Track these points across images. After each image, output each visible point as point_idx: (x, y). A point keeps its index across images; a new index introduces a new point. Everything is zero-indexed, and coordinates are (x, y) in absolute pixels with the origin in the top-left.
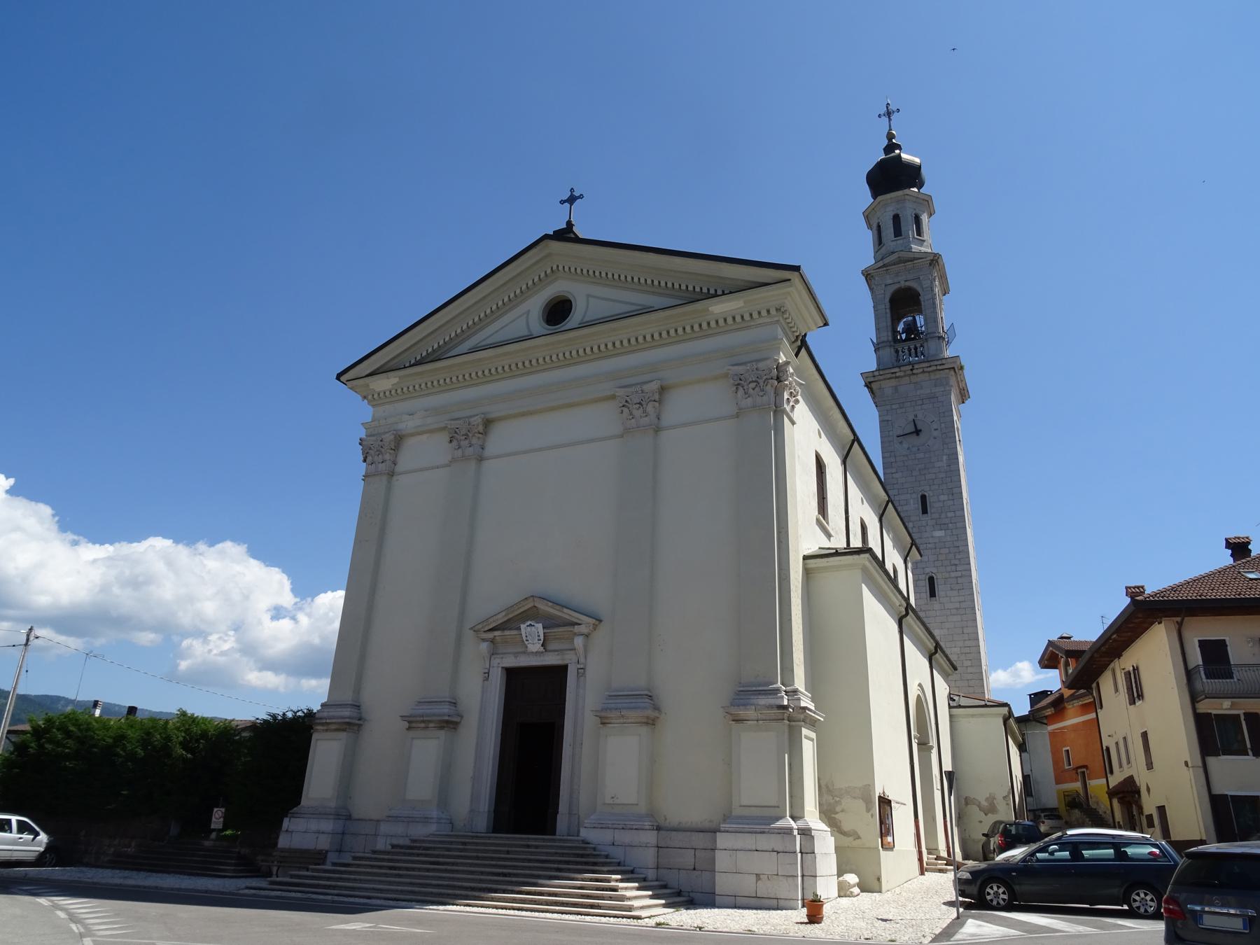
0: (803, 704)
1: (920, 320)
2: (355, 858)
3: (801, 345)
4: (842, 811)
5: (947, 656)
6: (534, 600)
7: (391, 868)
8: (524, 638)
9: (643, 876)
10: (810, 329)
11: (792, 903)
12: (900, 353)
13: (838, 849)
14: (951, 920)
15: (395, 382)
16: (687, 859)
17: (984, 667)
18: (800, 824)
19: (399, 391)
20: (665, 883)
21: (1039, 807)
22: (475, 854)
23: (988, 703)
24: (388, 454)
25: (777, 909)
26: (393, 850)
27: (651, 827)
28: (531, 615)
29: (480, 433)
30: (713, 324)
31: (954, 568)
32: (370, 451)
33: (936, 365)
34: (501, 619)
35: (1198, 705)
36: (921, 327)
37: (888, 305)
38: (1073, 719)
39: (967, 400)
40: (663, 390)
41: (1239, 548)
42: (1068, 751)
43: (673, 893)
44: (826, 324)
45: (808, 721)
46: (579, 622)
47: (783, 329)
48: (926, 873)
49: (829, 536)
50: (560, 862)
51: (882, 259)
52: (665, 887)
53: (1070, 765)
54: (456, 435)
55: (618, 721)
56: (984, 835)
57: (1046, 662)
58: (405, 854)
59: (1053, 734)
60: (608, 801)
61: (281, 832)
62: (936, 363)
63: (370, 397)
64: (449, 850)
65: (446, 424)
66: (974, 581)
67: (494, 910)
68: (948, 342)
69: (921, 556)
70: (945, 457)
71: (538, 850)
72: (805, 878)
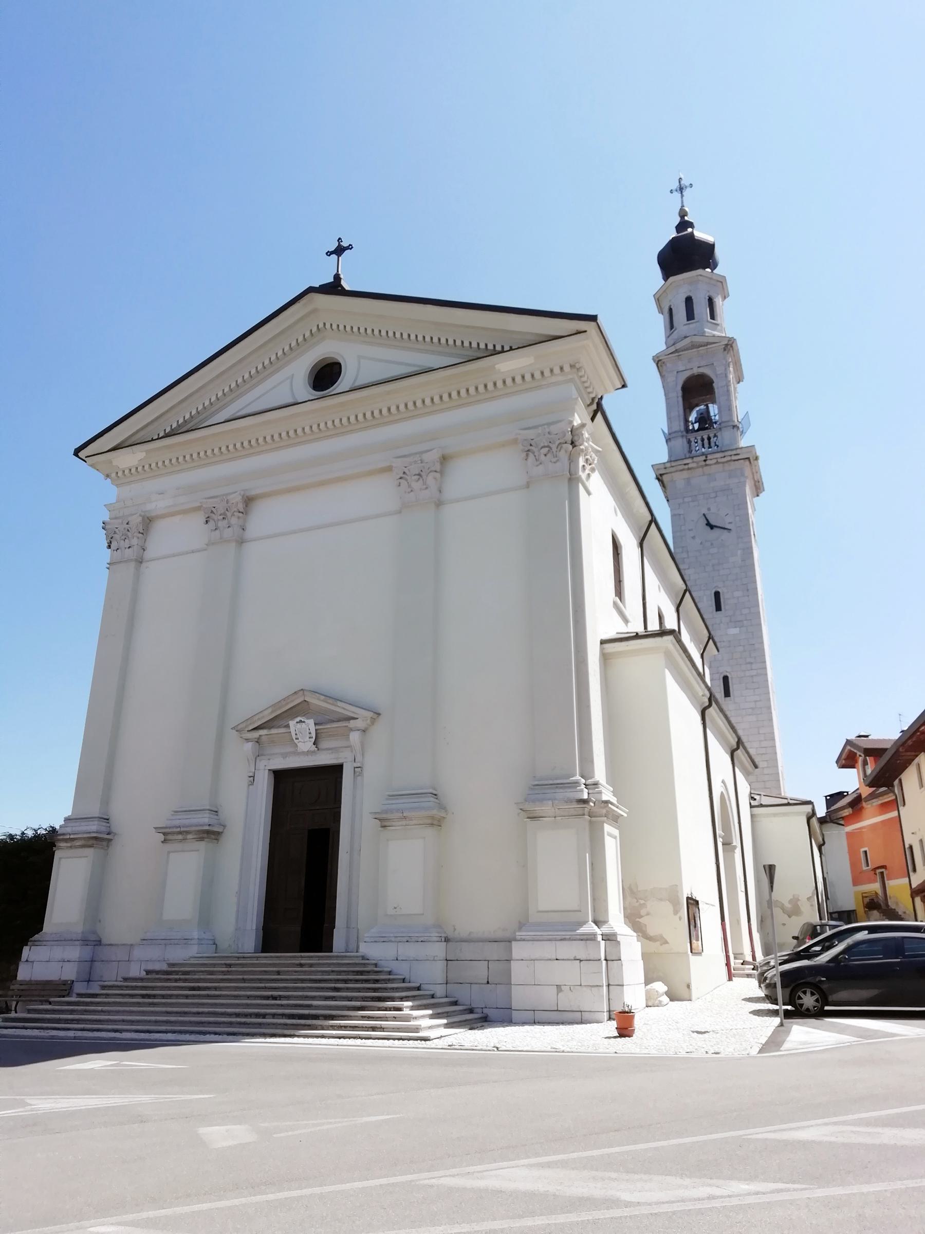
0: (605, 798)
1: (713, 409)
2: (103, 987)
3: (598, 409)
4: (648, 914)
5: (748, 753)
6: (304, 694)
7: (143, 996)
9: (432, 993)
10: (606, 391)
11: (597, 1016)
12: (693, 443)
13: (645, 956)
14: (774, 1028)
16: (479, 971)
17: (780, 768)
18: (605, 929)
19: (147, 467)
20: (455, 999)
21: (835, 910)
22: (241, 977)
23: (791, 802)
24: (135, 539)
25: (582, 1022)
26: (149, 976)
27: (438, 939)
28: (299, 710)
29: (239, 512)
30: (500, 384)
31: (749, 666)
32: (116, 535)
33: (731, 456)
36: (715, 416)
37: (680, 393)
38: (871, 819)
39: (761, 493)
40: (444, 459)
42: (866, 852)
43: (465, 1010)
44: (624, 386)
45: (610, 816)
46: (355, 716)
47: (578, 389)
48: (733, 978)
49: (626, 621)
50: (337, 981)
51: (674, 344)
52: (455, 1003)
53: (868, 865)
54: (212, 514)
56: (794, 938)
57: (844, 762)
58: (160, 980)
59: (849, 835)
60: (390, 911)
61: (20, 963)
62: (730, 453)
63: (113, 475)
64: (212, 973)
65: (201, 503)
66: (770, 680)
68: (742, 431)
69: (718, 651)
70: (739, 552)
71: (313, 969)
72: (610, 987)
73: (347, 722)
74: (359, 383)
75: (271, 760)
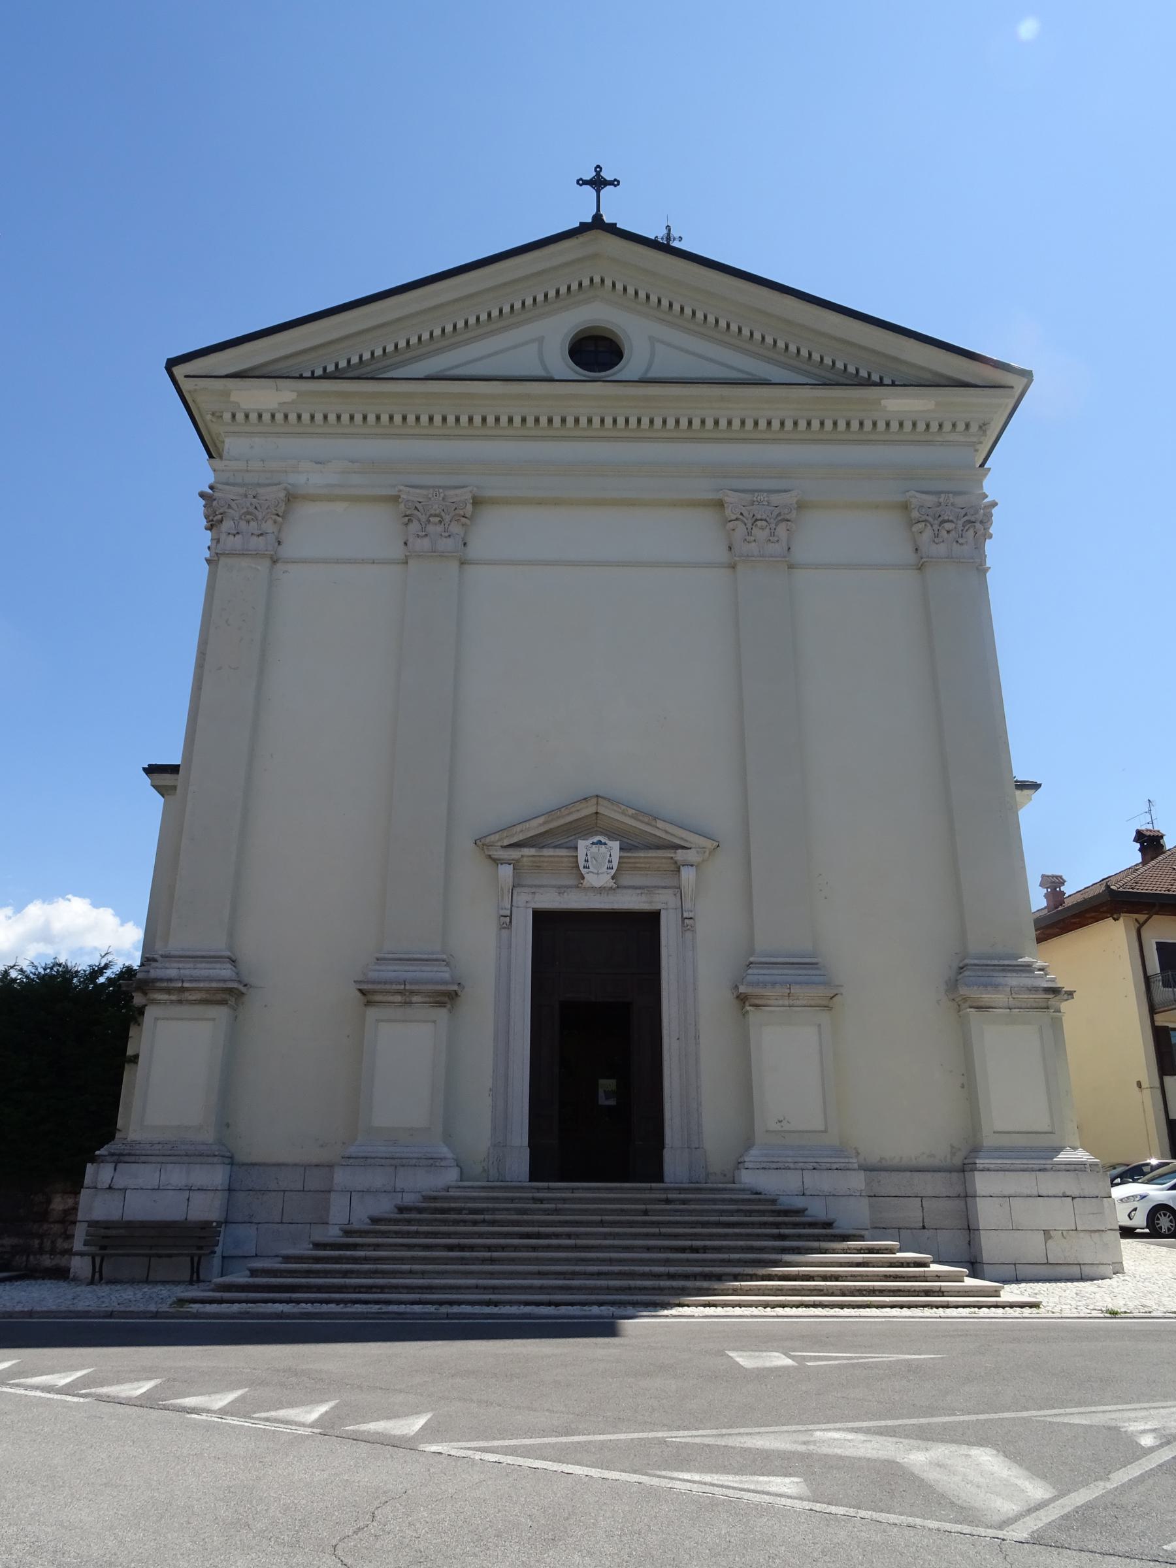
7: (451, 1248)
8: (581, 864)
15: (289, 400)
22: (598, 1218)
30: (881, 425)
32: (230, 511)
34: (535, 828)
35: (1157, 1017)
41: (1150, 843)
54: (416, 512)
55: (781, 1002)
60: (773, 1126)
65: (400, 491)
67: (837, 1310)
73: (673, 851)
74: (652, 374)
75: (537, 895)
